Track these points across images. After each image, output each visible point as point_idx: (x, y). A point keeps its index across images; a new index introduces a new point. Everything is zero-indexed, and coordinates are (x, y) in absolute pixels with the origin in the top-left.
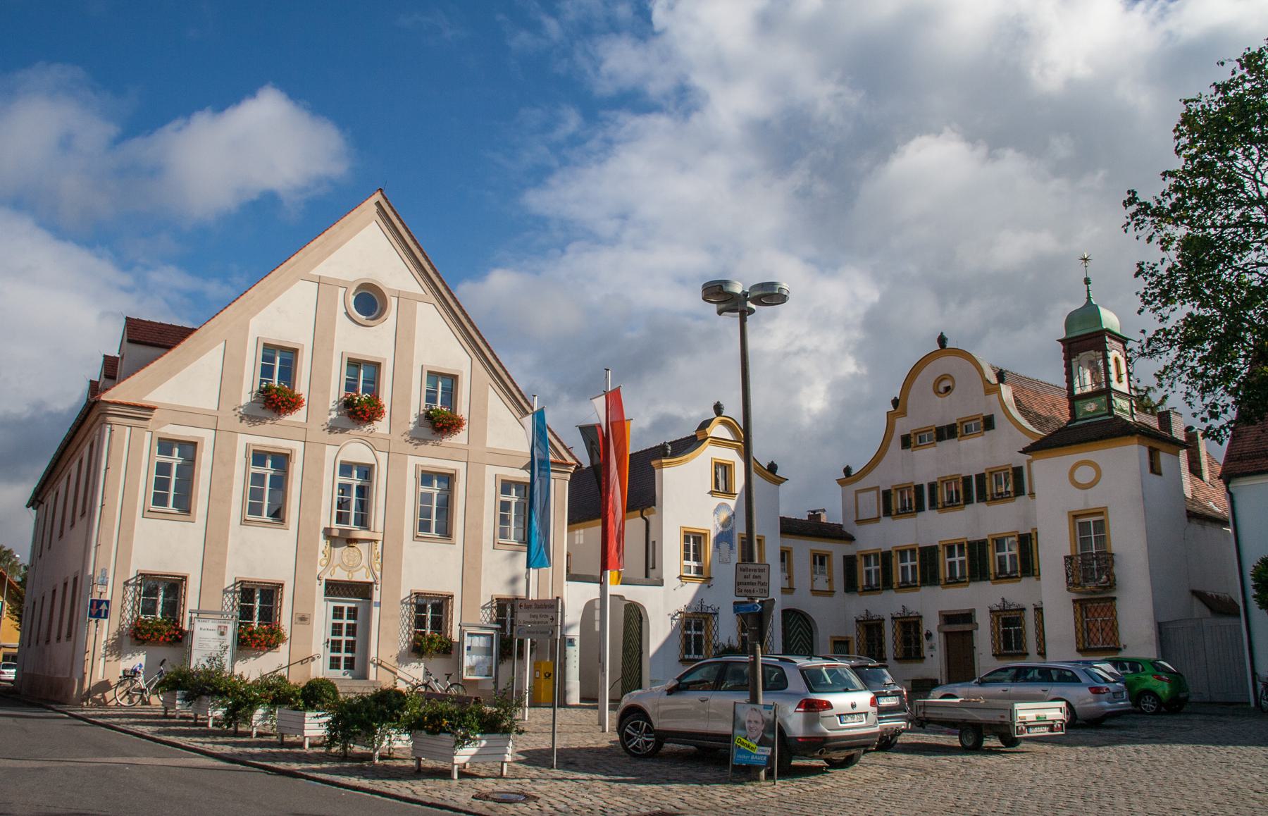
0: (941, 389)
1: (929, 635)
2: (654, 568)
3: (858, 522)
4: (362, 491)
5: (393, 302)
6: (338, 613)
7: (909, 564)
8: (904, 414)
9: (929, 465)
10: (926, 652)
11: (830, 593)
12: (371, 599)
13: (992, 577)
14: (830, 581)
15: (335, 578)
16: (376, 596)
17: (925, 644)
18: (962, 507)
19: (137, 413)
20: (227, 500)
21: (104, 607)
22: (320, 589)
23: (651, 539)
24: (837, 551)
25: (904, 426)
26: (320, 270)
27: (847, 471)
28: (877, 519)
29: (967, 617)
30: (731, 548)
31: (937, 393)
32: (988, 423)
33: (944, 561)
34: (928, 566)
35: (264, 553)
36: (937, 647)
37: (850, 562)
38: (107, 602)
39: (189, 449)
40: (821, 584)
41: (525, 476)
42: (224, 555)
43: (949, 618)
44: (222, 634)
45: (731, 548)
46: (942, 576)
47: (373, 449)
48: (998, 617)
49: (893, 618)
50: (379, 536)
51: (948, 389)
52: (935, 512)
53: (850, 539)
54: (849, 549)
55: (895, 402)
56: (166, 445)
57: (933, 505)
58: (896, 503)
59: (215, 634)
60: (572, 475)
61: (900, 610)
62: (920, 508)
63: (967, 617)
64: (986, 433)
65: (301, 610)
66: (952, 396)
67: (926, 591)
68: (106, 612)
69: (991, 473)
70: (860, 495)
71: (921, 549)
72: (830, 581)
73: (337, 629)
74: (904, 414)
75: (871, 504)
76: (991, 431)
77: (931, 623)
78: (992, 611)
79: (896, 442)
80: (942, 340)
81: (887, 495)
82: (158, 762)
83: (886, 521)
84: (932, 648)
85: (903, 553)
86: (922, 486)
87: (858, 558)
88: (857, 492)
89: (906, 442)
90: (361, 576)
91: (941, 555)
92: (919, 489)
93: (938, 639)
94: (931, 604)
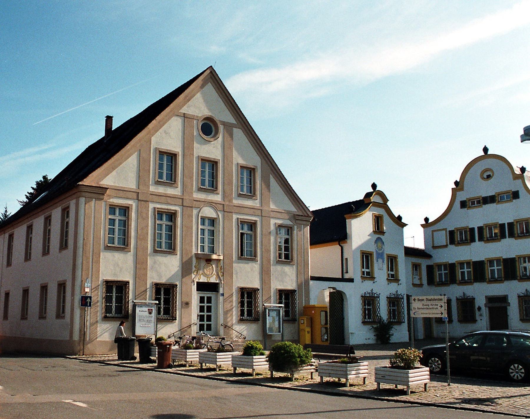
0: (485, 177)
1: (479, 309)
2: (347, 272)
3: (434, 247)
4: (212, 233)
5: (221, 128)
6: (202, 300)
7: (443, 272)
8: (462, 189)
9: (477, 218)
10: (478, 317)
11: (421, 285)
12: (218, 292)
13: (519, 278)
14: (420, 279)
15: (201, 281)
16: (221, 291)
17: (477, 313)
18: (499, 240)
19: (97, 190)
20: (145, 239)
21: (88, 300)
22: (194, 287)
23: (344, 258)
24: (424, 263)
25: (462, 196)
26: (184, 110)
27: (426, 220)
28: (446, 246)
29: (504, 299)
30: (383, 262)
31: (483, 178)
32: (516, 195)
33: (488, 270)
34: (479, 271)
35: (165, 268)
36: (484, 314)
37: (430, 269)
38: (90, 297)
39: (125, 210)
40: (417, 282)
41: (289, 223)
42: (146, 269)
43: (490, 300)
44: (150, 313)
45: (383, 262)
46: (487, 277)
47: (216, 210)
48: (522, 299)
49: (457, 299)
50: (221, 258)
51: (489, 177)
52: (482, 243)
53: (429, 256)
54: (429, 262)
55: (456, 183)
56: (112, 209)
57: (481, 239)
58: (458, 237)
59: (147, 314)
60: (311, 223)
61: (462, 295)
62: (473, 240)
63: (504, 299)
64: (514, 201)
65: (185, 300)
66: (492, 180)
67: (477, 285)
68: (90, 303)
69: (517, 222)
70: (435, 233)
71: (474, 262)
72: (420, 279)
73: (202, 309)
74: (462, 189)
75: (442, 238)
76: (517, 200)
77: (481, 302)
78: (519, 297)
79: (457, 204)
80: (485, 150)
81: (452, 233)
82: (429, 347)
83: (451, 247)
84: (481, 315)
85: (462, 264)
86: (473, 228)
87: (435, 266)
88: (433, 231)
89: (463, 204)
90: (213, 280)
91: (486, 266)
92: (472, 230)
93: (485, 311)
94: (480, 292)
